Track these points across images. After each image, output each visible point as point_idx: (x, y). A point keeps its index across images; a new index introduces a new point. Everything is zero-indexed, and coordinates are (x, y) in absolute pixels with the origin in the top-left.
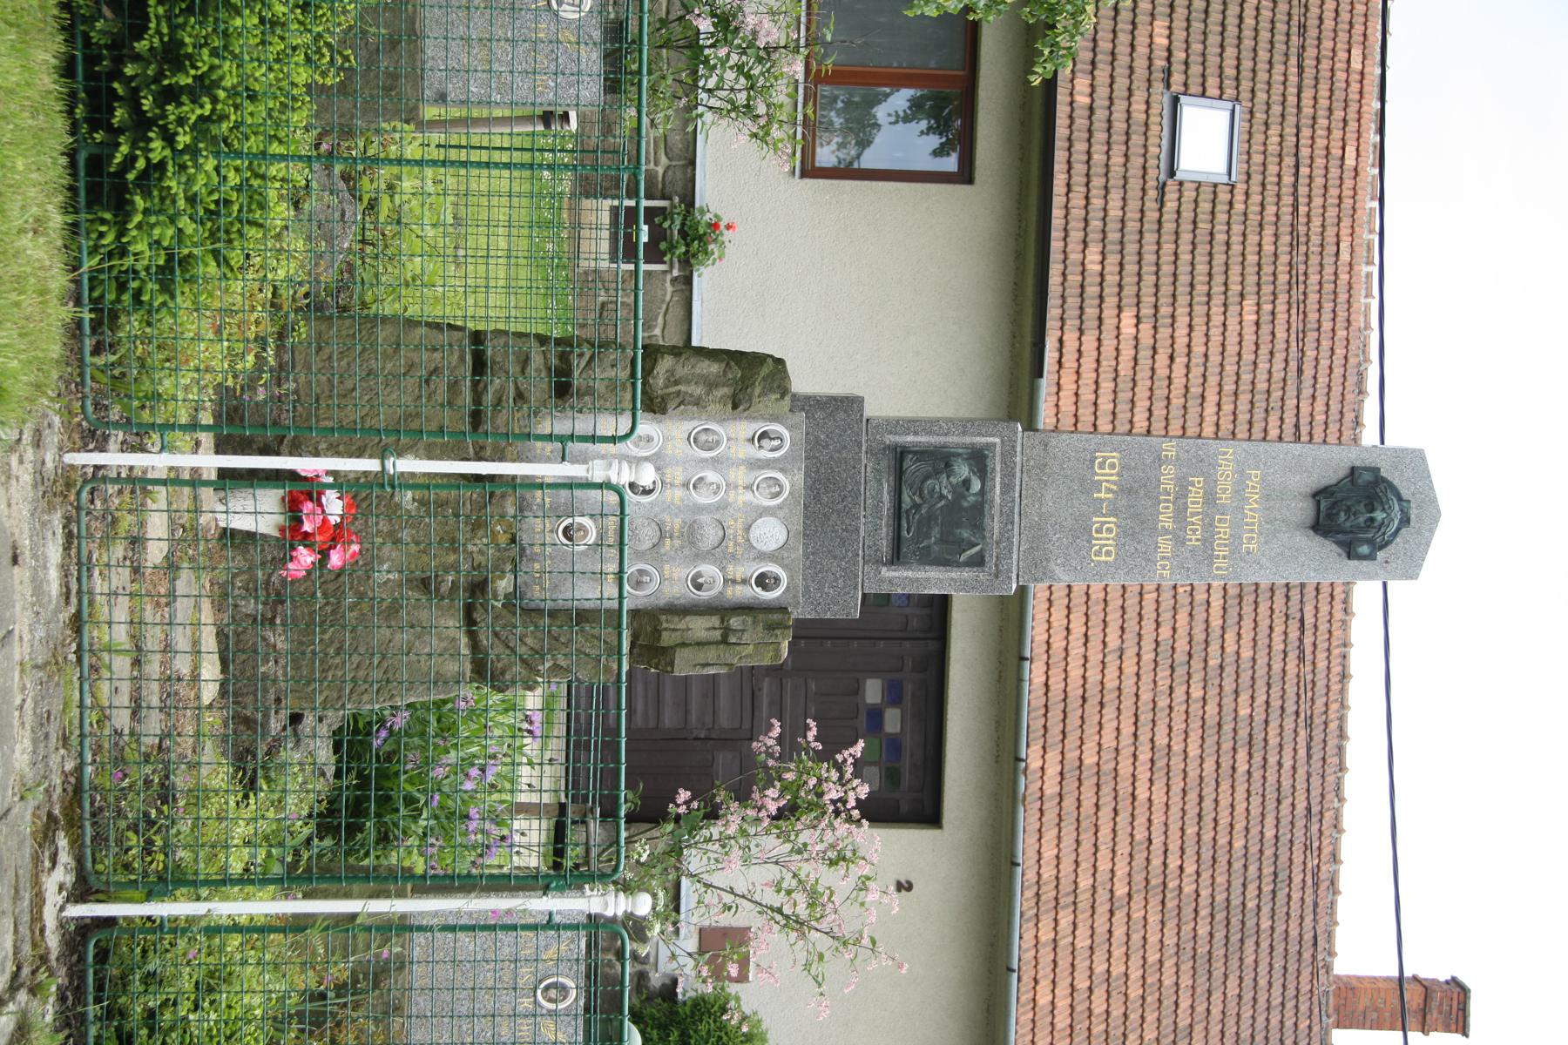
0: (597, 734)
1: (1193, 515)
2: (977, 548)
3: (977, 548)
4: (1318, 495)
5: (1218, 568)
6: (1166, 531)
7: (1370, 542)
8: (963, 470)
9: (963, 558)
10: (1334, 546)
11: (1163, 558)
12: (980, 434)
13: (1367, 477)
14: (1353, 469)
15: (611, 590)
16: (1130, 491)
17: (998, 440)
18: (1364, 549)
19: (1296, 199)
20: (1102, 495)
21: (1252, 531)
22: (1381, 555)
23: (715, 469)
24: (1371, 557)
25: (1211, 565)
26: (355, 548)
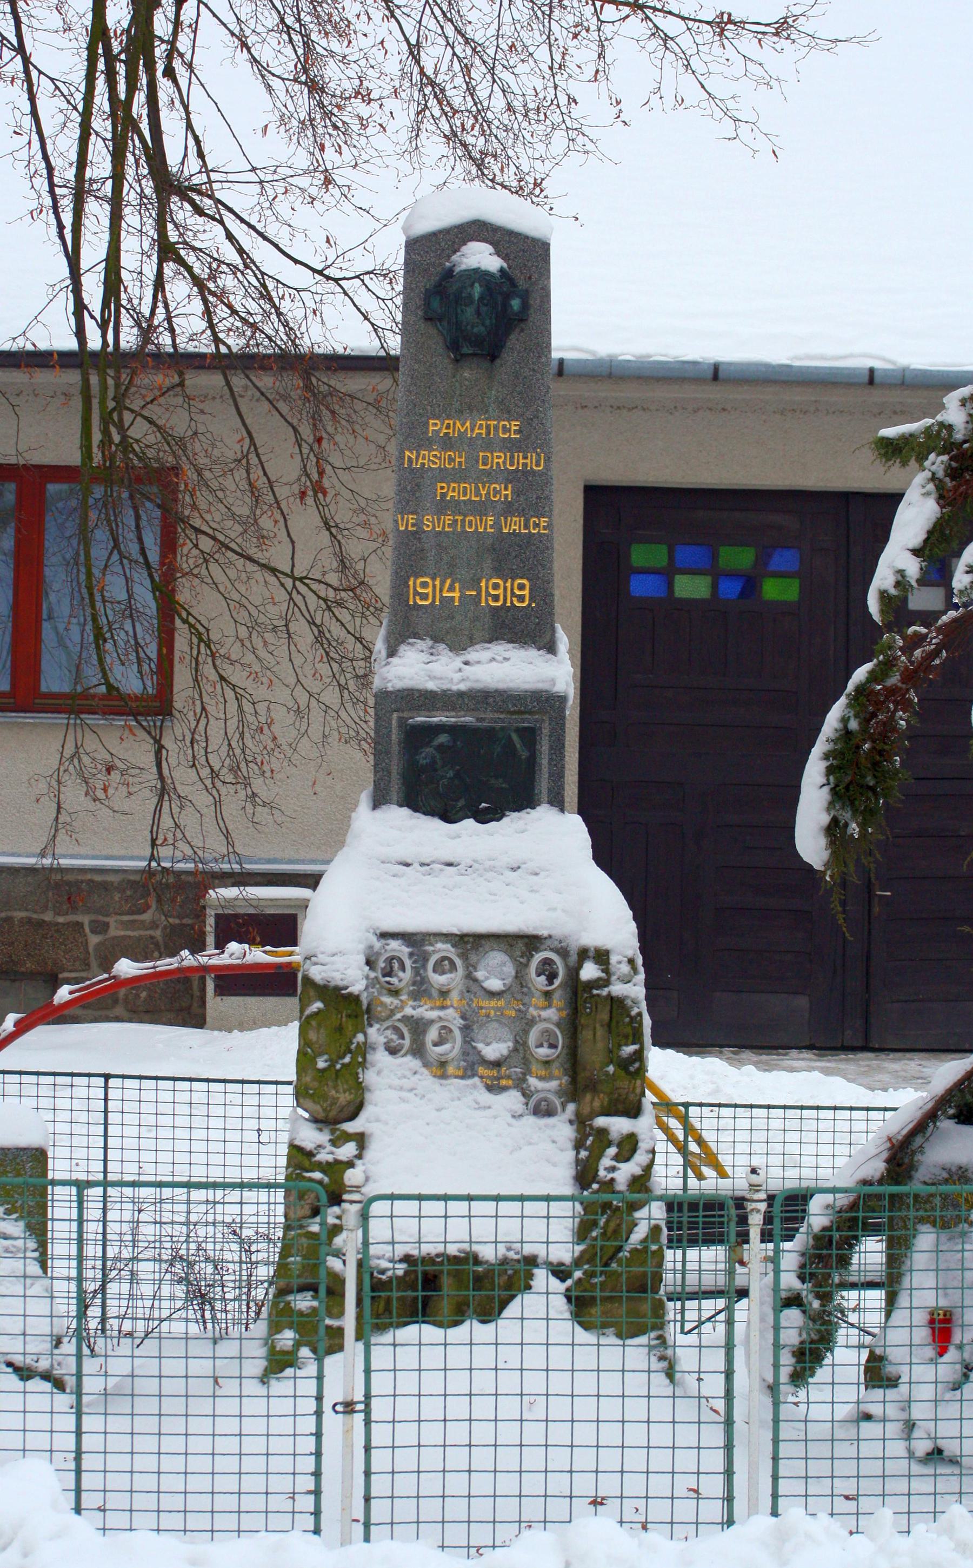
0: (714, 1216)
1: (478, 494)
2: (515, 737)
3: (515, 737)
4: (459, 359)
5: (538, 465)
6: (496, 525)
7: (507, 297)
8: (426, 755)
9: (524, 754)
10: (513, 337)
11: (526, 527)
12: (389, 736)
13: (436, 303)
14: (428, 319)
15: (557, 1208)
16: (452, 565)
17: (395, 715)
18: (516, 304)
19: (215, 1186)
20: (456, 594)
21: (496, 427)
22: (522, 284)
23: (424, 1032)
24: (525, 297)
25: (533, 472)
26: (881, 657)
